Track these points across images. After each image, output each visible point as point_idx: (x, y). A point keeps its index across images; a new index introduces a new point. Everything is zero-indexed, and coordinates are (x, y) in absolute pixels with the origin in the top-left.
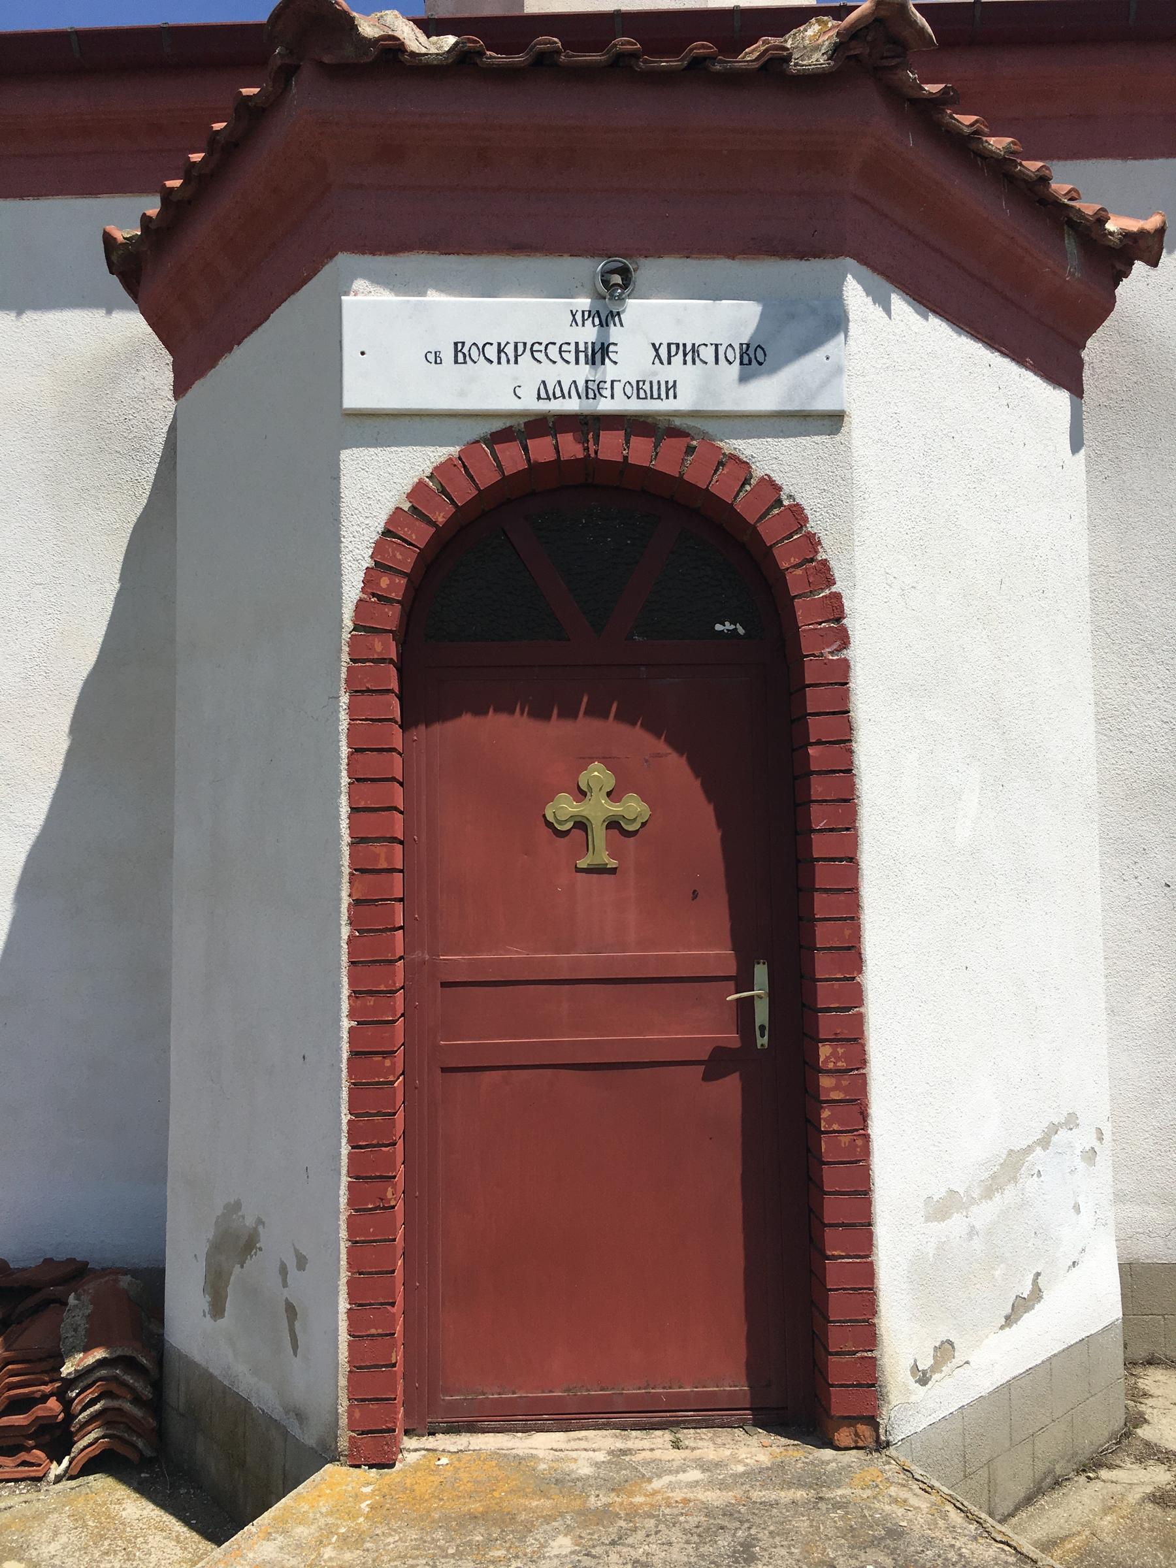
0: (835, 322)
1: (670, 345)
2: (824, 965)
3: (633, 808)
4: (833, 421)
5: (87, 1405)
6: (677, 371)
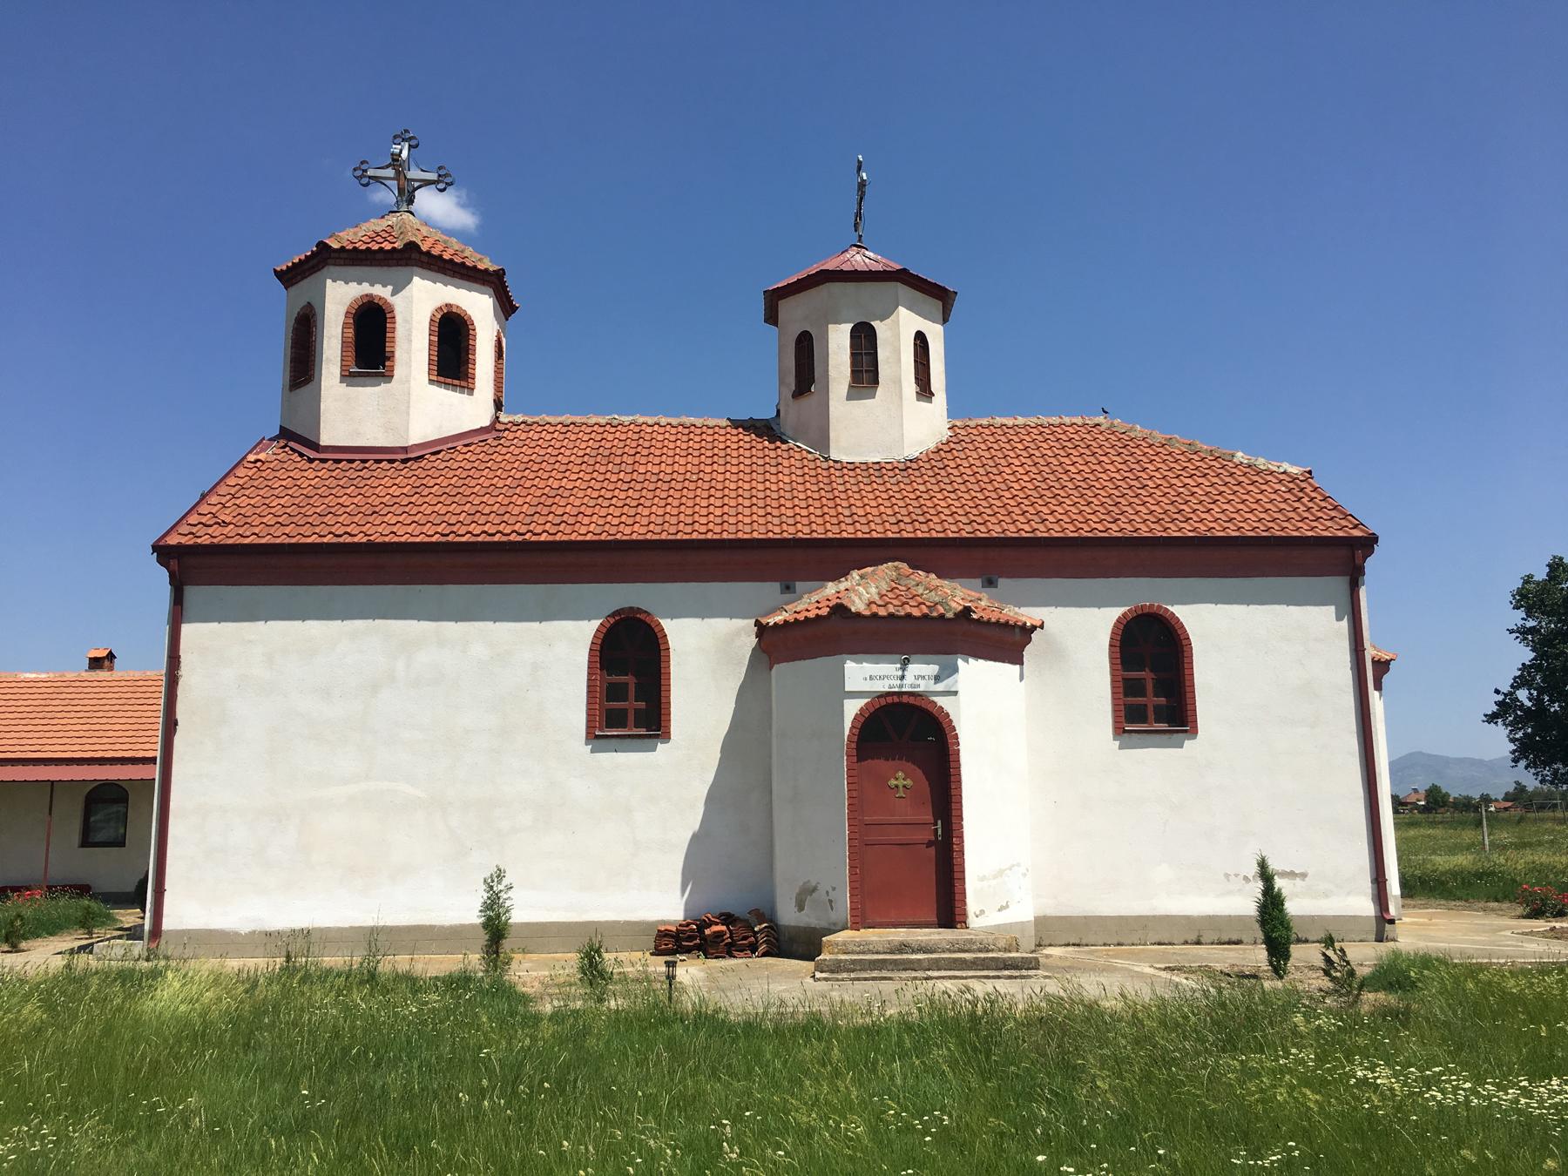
0: (956, 670)
1: (919, 675)
2: (954, 820)
3: (909, 782)
4: (956, 693)
5: (761, 938)
6: (920, 682)
